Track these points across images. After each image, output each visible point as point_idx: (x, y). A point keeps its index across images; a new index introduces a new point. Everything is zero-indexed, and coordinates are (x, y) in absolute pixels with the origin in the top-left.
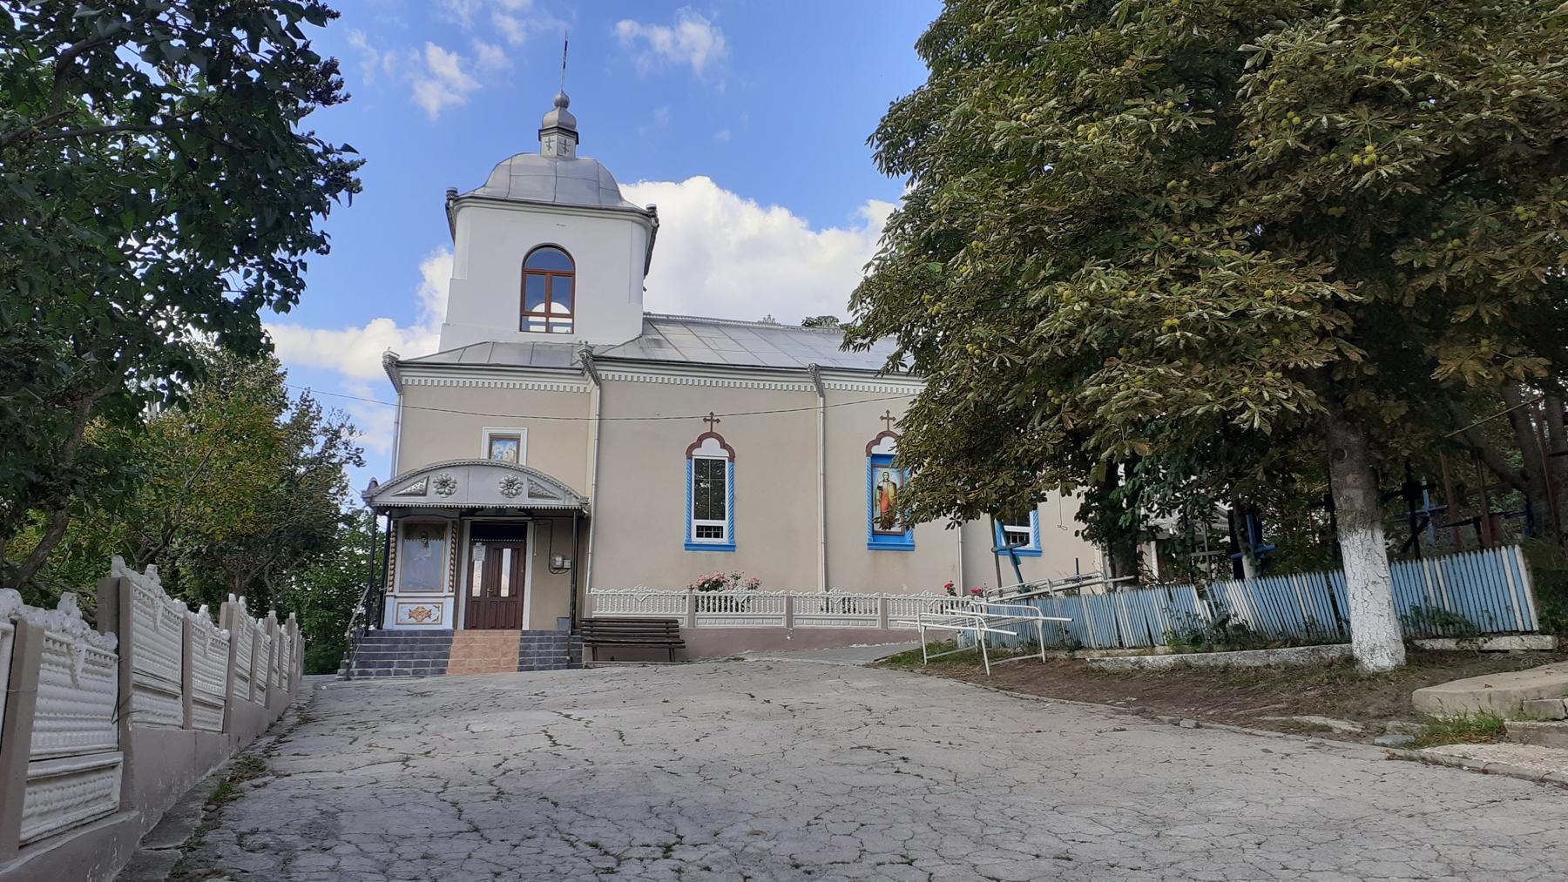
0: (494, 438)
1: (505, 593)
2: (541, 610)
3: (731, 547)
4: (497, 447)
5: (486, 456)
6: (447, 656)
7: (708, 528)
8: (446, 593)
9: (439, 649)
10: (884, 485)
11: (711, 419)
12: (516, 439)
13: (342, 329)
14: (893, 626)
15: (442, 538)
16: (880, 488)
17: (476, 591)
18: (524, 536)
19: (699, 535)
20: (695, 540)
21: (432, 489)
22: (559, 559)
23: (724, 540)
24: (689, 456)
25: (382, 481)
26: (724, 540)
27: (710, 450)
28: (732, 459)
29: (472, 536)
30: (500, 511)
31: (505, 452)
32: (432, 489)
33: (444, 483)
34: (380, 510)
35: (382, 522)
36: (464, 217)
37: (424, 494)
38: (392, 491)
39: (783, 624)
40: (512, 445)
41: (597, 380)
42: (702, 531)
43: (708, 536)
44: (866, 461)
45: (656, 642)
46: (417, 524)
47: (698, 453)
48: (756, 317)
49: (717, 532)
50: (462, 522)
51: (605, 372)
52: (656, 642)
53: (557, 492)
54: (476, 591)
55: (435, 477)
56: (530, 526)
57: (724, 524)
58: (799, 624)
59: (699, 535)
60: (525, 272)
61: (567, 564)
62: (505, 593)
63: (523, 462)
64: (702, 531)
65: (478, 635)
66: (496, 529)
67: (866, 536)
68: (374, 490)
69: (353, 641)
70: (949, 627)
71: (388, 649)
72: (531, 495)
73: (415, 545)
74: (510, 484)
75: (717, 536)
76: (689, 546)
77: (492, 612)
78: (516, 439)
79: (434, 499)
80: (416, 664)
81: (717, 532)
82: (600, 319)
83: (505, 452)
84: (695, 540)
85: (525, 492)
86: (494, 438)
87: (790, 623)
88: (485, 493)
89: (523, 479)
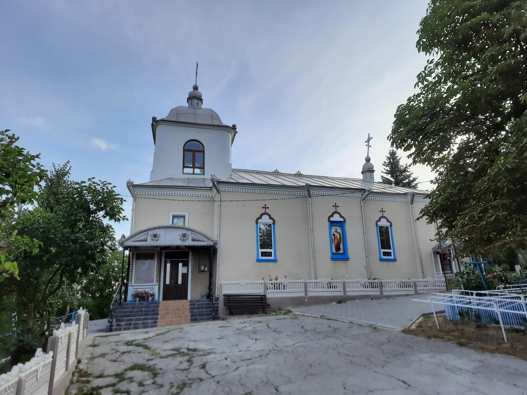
0: (174, 217)
1: (180, 282)
2: (195, 291)
3: (275, 261)
4: (176, 220)
5: (171, 224)
6: (157, 314)
7: (266, 252)
8: (154, 283)
9: (154, 311)
10: (336, 234)
11: (265, 207)
12: (184, 217)
13: (395, 116)
14: (349, 294)
15: (153, 261)
16: (334, 235)
17: (168, 282)
18: (188, 257)
19: (262, 256)
20: (261, 258)
21: (149, 238)
22: (203, 267)
23: (272, 258)
24: (377, 225)
25: (127, 235)
26: (272, 258)
27: (383, 223)
28: (391, 226)
29: (165, 258)
30: (178, 247)
31: (179, 222)
32: (149, 238)
33: (155, 236)
34: (126, 248)
35: (127, 252)
36: (160, 129)
37: (146, 241)
38: (136, 238)
39: (303, 294)
40: (182, 219)
41: (218, 191)
42: (264, 254)
43: (266, 256)
44: (327, 224)
45: (250, 306)
46: (141, 253)
47: (380, 224)
48: (272, 170)
49: (270, 254)
50: (161, 252)
51: (221, 187)
52: (250, 306)
53: (204, 239)
54: (168, 282)
55: (151, 233)
56: (190, 253)
57: (272, 250)
58: (310, 294)
59: (262, 256)
60: (184, 150)
61: (206, 269)
62: (180, 282)
63: (186, 225)
64: (264, 254)
65: (165, 302)
66: (175, 255)
67: (329, 255)
68: (123, 240)
69: (114, 310)
70: (441, 303)
71: (130, 312)
72: (193, 240)
73: (141, 262)
74: (184, 235)
75: (269, 256)
76: (258, 261)
77: (175, 291)
78: (184, 217)
79: (150, 243)
80: (144, 319)
81: (270, 254)
82: (213, 169)
83: (179, 222)
84: (261, 258)
85: (190, 238)
86: (174, 217)
87: (306, 294)
88: (171, 239)
89: (189, 233)
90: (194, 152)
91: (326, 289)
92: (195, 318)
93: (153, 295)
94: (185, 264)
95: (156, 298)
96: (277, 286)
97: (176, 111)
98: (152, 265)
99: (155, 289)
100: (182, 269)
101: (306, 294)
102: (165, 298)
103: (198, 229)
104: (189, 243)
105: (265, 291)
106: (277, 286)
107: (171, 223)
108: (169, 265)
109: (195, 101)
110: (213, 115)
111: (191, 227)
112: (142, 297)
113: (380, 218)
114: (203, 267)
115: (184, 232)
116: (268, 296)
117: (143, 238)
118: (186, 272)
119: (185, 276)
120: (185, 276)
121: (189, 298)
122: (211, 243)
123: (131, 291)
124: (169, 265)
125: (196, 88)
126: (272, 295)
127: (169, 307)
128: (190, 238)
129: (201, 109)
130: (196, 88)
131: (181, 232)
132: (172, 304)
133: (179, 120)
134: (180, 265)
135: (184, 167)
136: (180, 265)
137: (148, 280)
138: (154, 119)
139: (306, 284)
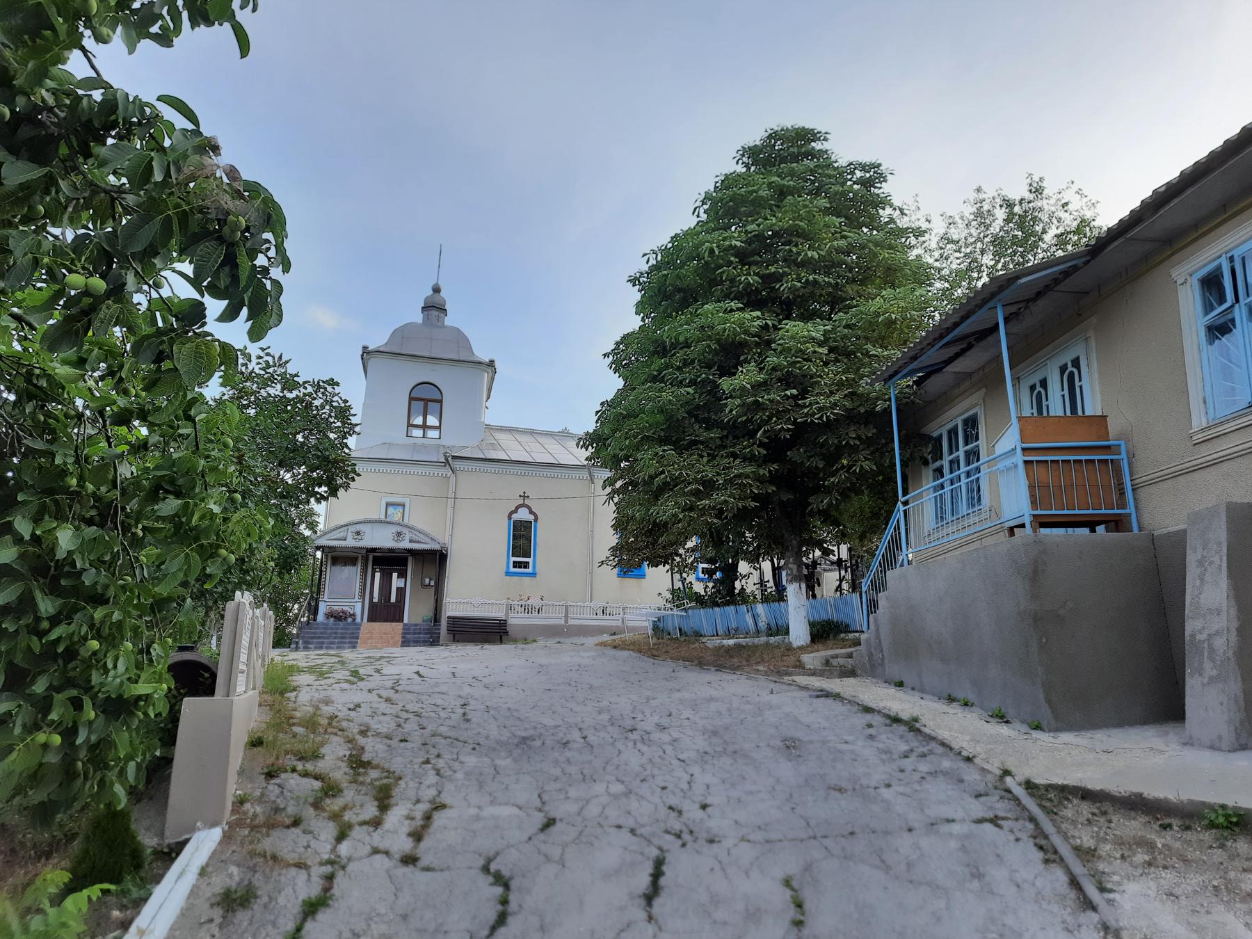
0: (388, 505)
1: (393, 599)
2: (415, 612)
3: (533, 575)
4: (391, 510)
11: (524, 497)
17: (376, 600)
22: (427, 580)
23: (530, 570)
24: (510, 517)
26: (530, 570)
27: (523, 515)
28: (536, 520)
30: (391, 550)
31: (395, 514)
33: (358, 533)
35: (319, 554)
39: (562, 622)
40: (400, 509)
42: (516, 565)
45: (489, 632)
46: (339, 557)
49: (526, 565)
51: (457, 464)
52: (489, 632)
53: (427, 540)
54: (376, 600)
55: (353, 529)
56: (410, 559)
58: (571, 622)
60: (411, 399)
61: (432, 583)
62: (393, 599)
64: (516, 565)
65: (377, 625)
66: (388, 561)
72: (411, 541)
73: (337, 569)
74: (399, 534)
76: (508, 573)
77: (386, 611)
79: (351, 542)
81: (526, 565)
83: (395, 514)
84: (512, 569)
85: (407, 538)
87: (566, 621)
88: (382, 539)
89: (405, 530)
90: (426, 401)
91: (600, 616)
92: (405, 643)
93: (353, 615)
94: (402, 575)
95: (358, 620)
96: (528, 609)
97: (402, 333)
98: (352, 574)
99: (358, 608)
100: (396, 582)
101: (566, 621)
102: (371, 619)
103: (420, 526)
104: (405, 544)
105: (507, 614)
106: (528, 609)
107: (383, 517)
108: (378, 575)
109: (434, 313)
110: (461, 340)
111: (413, 523)
112: (338, 616)
113: (517, 508)
114: (427, 580)
115: (399, 529)
116: (511, 621)
117: (341, 535)
118: (402, 585)
119: (401, 592)
120: (401, 592)
121: (406, 621)
122: (437, 547)
123: (323, 608)
124: (378, 575)
125: (436, 290)
126: (516, 620)
127: (369, 629)
128: (407, 538)
129: (444, 327)
130: (436, 290)
131: (395, 529)
132: (379, 627)
133: (403, 352)
134: (395, 575)
135: (410, 425)
136: (395, 575)
137: (345, 592)
138: (365, 348)
139: (567, 607)
